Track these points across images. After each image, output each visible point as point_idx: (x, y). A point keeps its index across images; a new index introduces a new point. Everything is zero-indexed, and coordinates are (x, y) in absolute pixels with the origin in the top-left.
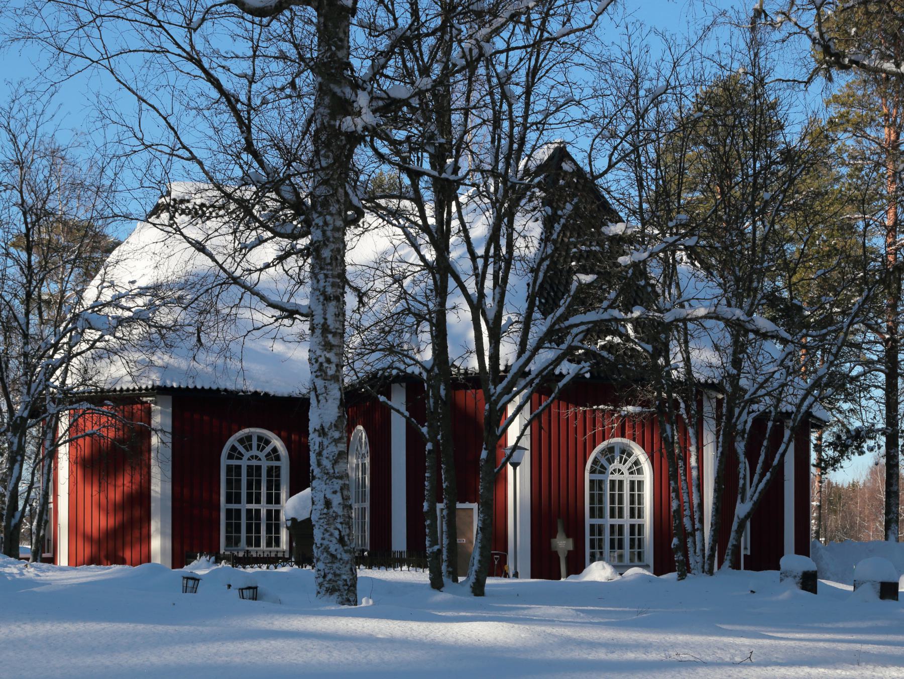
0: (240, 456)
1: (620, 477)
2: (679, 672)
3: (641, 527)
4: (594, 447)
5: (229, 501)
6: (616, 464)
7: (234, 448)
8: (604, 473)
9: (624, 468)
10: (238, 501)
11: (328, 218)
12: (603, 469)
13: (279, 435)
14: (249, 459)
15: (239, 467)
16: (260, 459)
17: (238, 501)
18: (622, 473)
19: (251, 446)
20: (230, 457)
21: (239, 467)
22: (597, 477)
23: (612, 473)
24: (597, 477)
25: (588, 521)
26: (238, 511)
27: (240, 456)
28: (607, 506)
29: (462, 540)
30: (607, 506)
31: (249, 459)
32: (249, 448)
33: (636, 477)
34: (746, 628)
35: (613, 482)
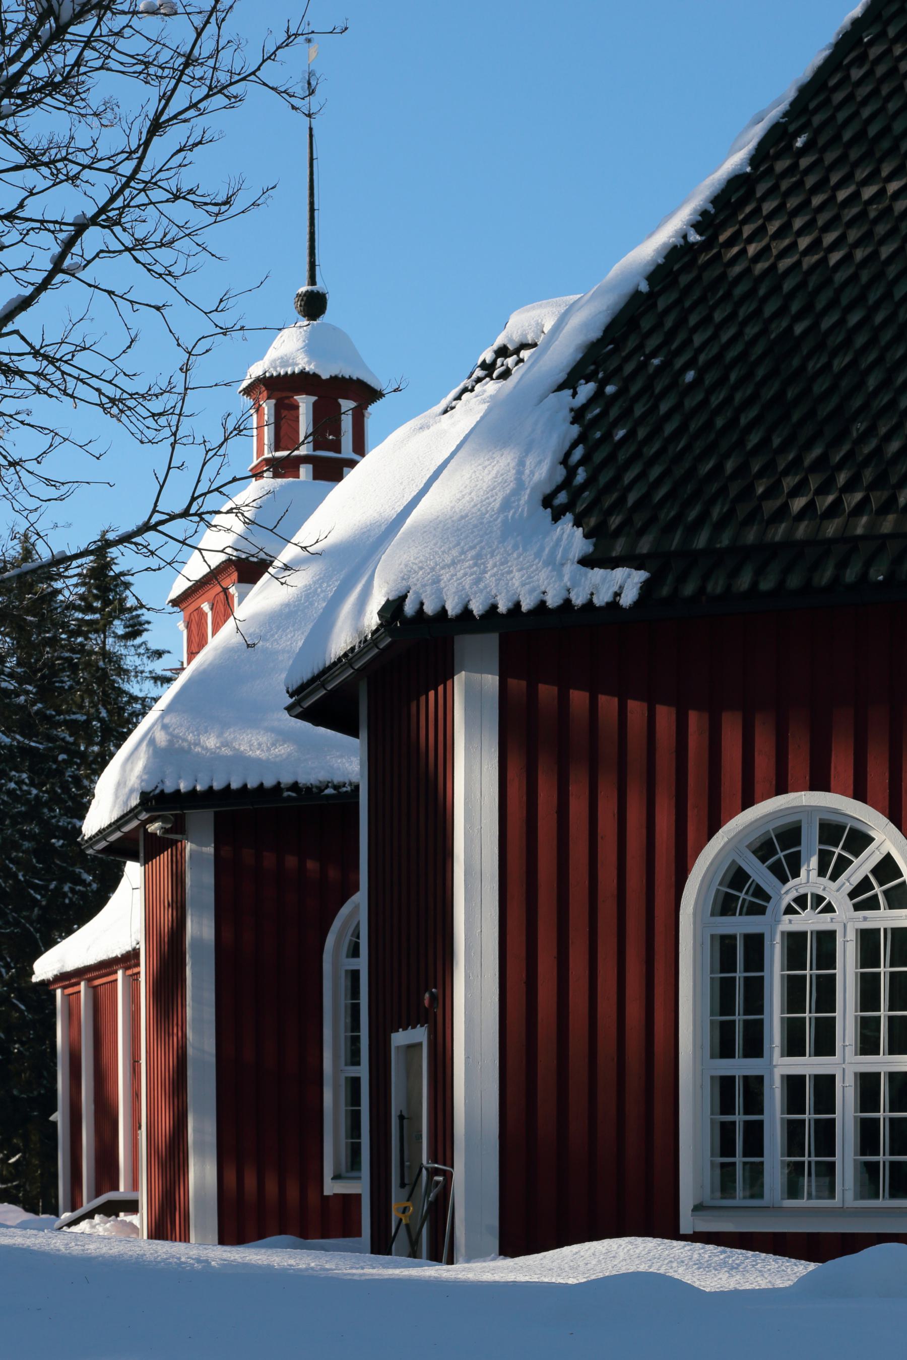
1: (822, 922)
4: (713, 828)
16: (829, 909)
18: (829, 909)
23: (789, 910)
35: (795, 941)
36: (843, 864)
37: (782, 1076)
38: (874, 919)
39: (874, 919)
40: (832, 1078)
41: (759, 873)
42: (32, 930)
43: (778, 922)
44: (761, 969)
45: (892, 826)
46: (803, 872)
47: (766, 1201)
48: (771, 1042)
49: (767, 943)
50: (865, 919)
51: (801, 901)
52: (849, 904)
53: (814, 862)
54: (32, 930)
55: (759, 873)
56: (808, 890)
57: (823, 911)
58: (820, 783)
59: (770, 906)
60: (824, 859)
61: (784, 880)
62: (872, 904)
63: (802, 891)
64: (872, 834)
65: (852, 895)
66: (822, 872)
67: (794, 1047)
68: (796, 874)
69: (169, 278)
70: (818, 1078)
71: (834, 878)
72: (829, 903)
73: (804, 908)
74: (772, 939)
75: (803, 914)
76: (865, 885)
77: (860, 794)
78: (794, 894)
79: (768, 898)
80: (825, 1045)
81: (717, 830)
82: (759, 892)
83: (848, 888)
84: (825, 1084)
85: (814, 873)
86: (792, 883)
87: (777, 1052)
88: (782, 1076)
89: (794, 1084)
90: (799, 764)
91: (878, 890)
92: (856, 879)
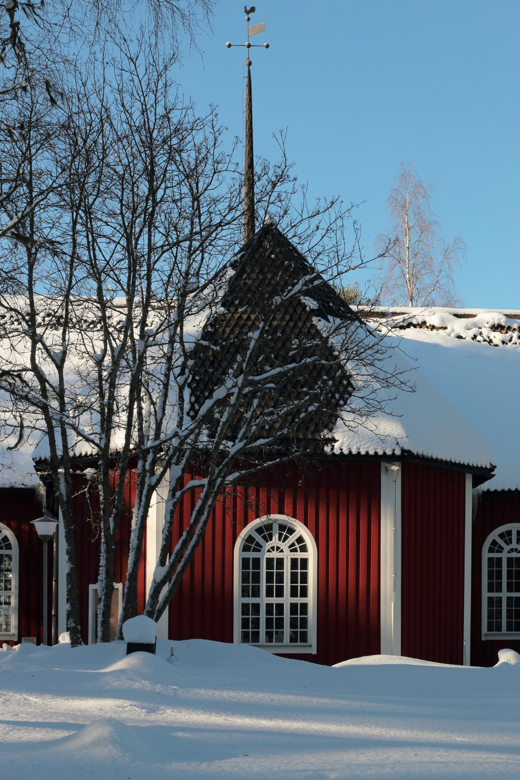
0: (500, 549)
1: (280, 555)
2: (349, 731)
3: (304, 606)
4: (246, 524)
5: (490, 590)
6: (275, 541)
7: (494, 543)
8: (260, 551)
9: (285, 546)
10: (499, 590)
11: (14, 262)
12: (258, 548)
13: (9, 525)
14: (509, 552)
15: (500, 560)
16: (282, 551)
17: (499, 590)
18: (282, 551)
19: (511, 540)
20: (491, 550)
21: (500, 560)
22: (251, 555)
23: (269, 551)
24: (251, 555)
25: (238, 599)
26: (500, 599)
27: (500, 549)
28: (263, 584)
29: (112, 620)
30: (263, 584)
31: (509, 552)
32: (509, 542)
33: (299, 555)
34: (247, 696)
35: (270, 561)
36: (286, 538)
37: (93, 590)
38: (297, 555)
39: (297, 555)
40: (283, 604)
41: (258, 538)
42: (102, 534)
43: (264, 554)
44: (259, 569)
45: (305, 527)
46: (274, 538)
47: (284, 643)
48: (263, 592)
49: (261, 561)
50: (294, 555)
51: (273, 548)
52: (289, 550)
53: (277, 536)
54: (102, 534)
55: (258, 538)
56: (275, 545)
57: (280, 552)
58: (281, 512)
59: (262, 550)
60: (280, 535)
61: (267, 541)
62: (295, 550)
63: (273, 545)
64: (296, 528)
65: (289, 547)
66: (280, 540)
67: (269, 594)
68: (271, 540)
69: (357, 242)
70: (277, 605)
71: (284, 541)
72: (282, 550)
73: (513, 552)
74: (263, 560)
75: (273, 552)
76: (293, 545)
77: (294, 516)
78: (271, 546)
79: (261, 547)
80: (280, 593)
81: (247, 524)
82: (258, 544)
83: (289, 545)
84: (280, 607)
85: (277, 540)
86: (270, 542)
87: (265, 595)
88: (93, 590)
89: (269, 606)
90: (274, 504)
91: (253, 546)
92: (291, 543)
